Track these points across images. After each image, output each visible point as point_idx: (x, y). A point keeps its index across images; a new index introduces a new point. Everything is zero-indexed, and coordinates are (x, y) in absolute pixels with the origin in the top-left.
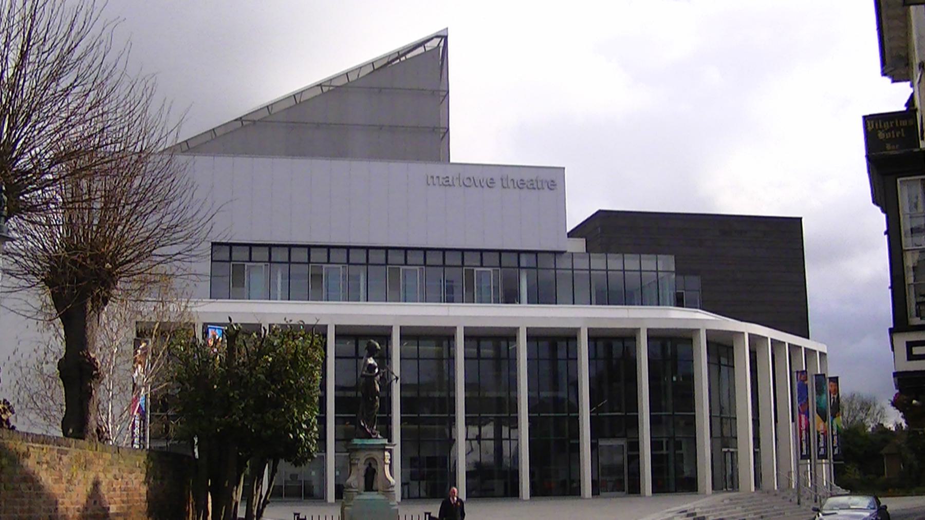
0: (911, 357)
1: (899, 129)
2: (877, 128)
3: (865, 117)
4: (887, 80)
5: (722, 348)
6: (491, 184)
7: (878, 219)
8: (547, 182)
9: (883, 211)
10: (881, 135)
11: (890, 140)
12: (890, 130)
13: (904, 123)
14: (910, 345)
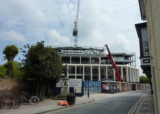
0: (144, 63)
14: (144, 60)
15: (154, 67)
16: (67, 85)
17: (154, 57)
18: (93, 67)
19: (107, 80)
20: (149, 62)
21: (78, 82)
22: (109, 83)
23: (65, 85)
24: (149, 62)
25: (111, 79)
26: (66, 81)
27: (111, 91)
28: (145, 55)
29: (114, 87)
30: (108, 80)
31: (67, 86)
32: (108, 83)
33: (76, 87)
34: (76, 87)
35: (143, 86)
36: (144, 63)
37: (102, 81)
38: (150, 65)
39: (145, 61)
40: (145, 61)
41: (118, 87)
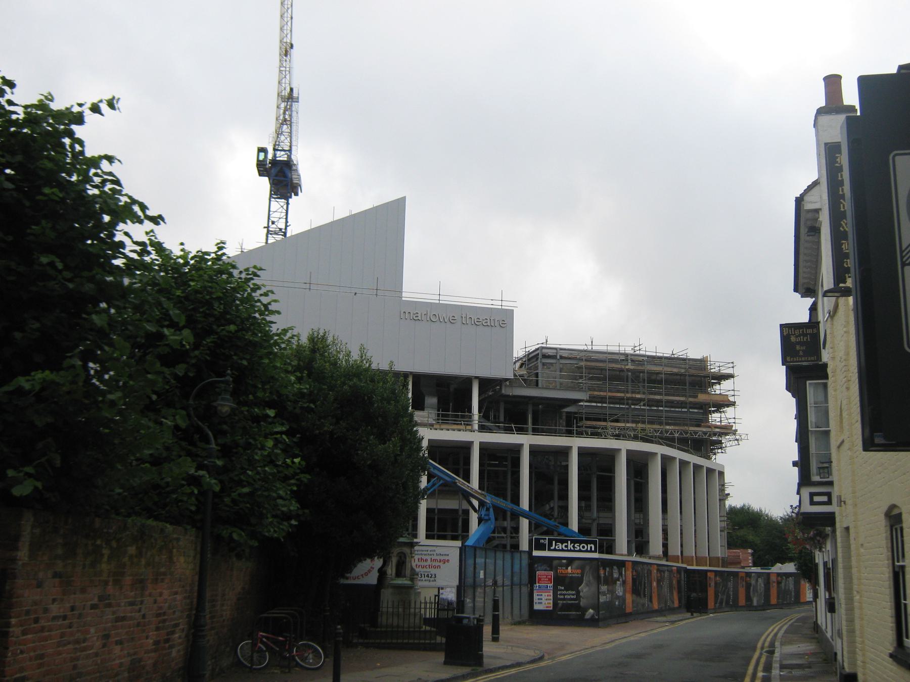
0: (812, 503)
1: (806, 335)
2: (789, 333)
3: (781, 325)
4: (798, 295)
5: (638, 467)
6: (452, 321)
7: (790, 402)
8: (499, 321)
9: (793, 396)
10: (793, 339)
11: (798, 343)
12: (800, 335)
13: (809, 331)
14: (812, 495)
15: (847, 529)
16: (408, 572)
17: (849, 502)
18: (628, 451)
19: (560, 546)
20: (829, 502)
21: (438, 558)
22: (576, 563)
23: (399, 574)
24: (829, 502)
25: (587, 542)
26: (406, 550)
27: (585, 610)
28: (816, 478)
29: (604, 588)
30: (570, 546)
31: (412, 580)
32: (571, 560)
33: (427, 583)
34: (427, 583)
35: (748, 586)
36: (812, 503)
37: (536, 553)
38: (834, 513)
39: (816, 499)
40: (816, 499)
41: (619, 591)
